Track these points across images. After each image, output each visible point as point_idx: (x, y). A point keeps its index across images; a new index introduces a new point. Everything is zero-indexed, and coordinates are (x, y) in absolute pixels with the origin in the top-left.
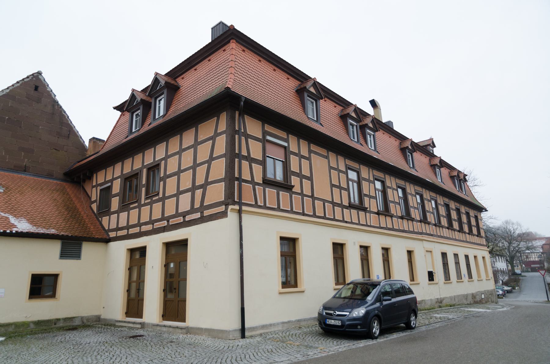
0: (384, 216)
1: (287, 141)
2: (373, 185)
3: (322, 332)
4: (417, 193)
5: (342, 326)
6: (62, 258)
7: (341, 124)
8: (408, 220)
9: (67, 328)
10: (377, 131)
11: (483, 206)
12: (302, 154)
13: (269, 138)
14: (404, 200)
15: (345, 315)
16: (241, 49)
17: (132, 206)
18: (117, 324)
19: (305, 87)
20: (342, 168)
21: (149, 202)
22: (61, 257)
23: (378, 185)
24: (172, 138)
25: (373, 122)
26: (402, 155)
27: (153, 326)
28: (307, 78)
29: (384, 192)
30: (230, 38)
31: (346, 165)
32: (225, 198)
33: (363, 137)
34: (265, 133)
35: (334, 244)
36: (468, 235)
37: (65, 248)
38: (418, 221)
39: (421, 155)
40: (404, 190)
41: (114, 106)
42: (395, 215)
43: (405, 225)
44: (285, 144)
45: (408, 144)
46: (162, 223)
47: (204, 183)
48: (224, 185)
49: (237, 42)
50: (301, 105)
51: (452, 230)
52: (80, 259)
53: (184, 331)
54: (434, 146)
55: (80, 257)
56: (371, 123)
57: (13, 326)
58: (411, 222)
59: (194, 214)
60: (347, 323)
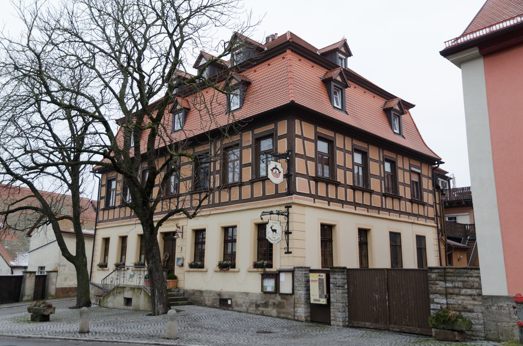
0: (325, 184)
1: (420, 168)
2: (351, 155)
3: (106, 302)
4: (387, 160)
7: (384, 118)
8: (393, 198)
10: (404, 114)
11: (438, 157)
12: (346, 149)
13: (413, 169)
14: (363, 168)
16: (298, 59)
19: (332, 78)
20: (349, 148)
23: (358, 158)
25: (399, 104)
26: (386, 119)
28: (410, 106)
29: (365, 166)
31: (316, 132)
33: (388, 121)
34: (410, 166)
35: (391, 233)
36: (410, 203)
38: (406, 200)
39: (355, 88)
40: (365, 155)
42: (343, 182)
43: (416, 209)
44: (419, 171)
45: (394, 104)
48: (299, 178)
49: (292, 51)
50: (327, 94)
51: (418, 205)
54: (348, 54)
56: (339, 76)
58: (398, 201)
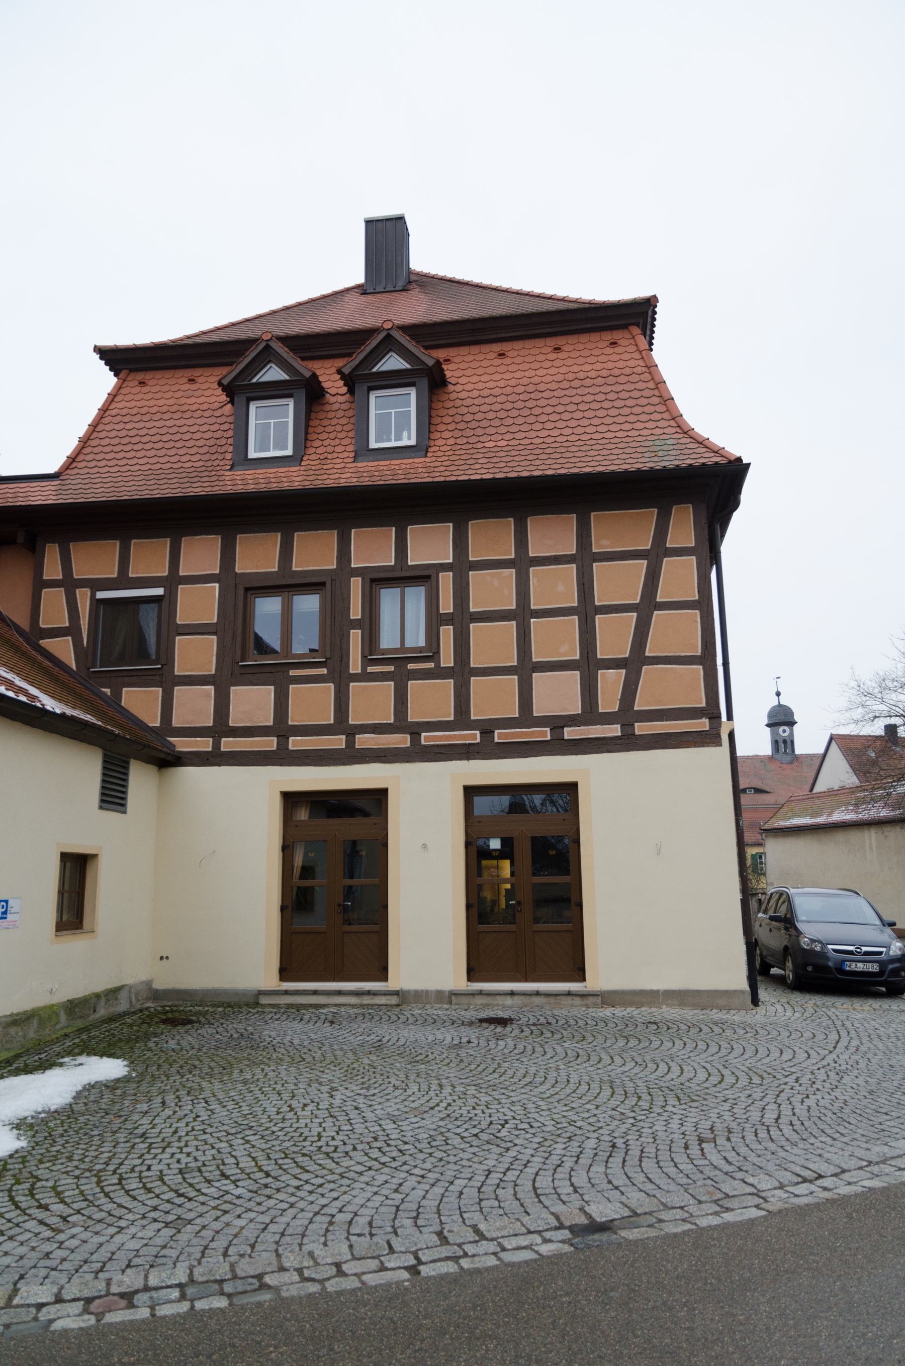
5: (881, 973)
6: (104, 805)
9: (591, 1000)
15: (880, 953)
17: (292, 673)
18: (264, 1000)
21: (389, 672)
22: (102, 801)
24: (481, 518)
27: (453, 997)
30: (633, 321)
32: (179, 676)
37: (113, 770)
41: (99, 344)
46: (460, 735)
47: (627, 655)
52: (125, 812)
53: (598, 1000)
55: (123, 805)
57: (35, 1022)
59: (599, 727)
60: (891, 967)
